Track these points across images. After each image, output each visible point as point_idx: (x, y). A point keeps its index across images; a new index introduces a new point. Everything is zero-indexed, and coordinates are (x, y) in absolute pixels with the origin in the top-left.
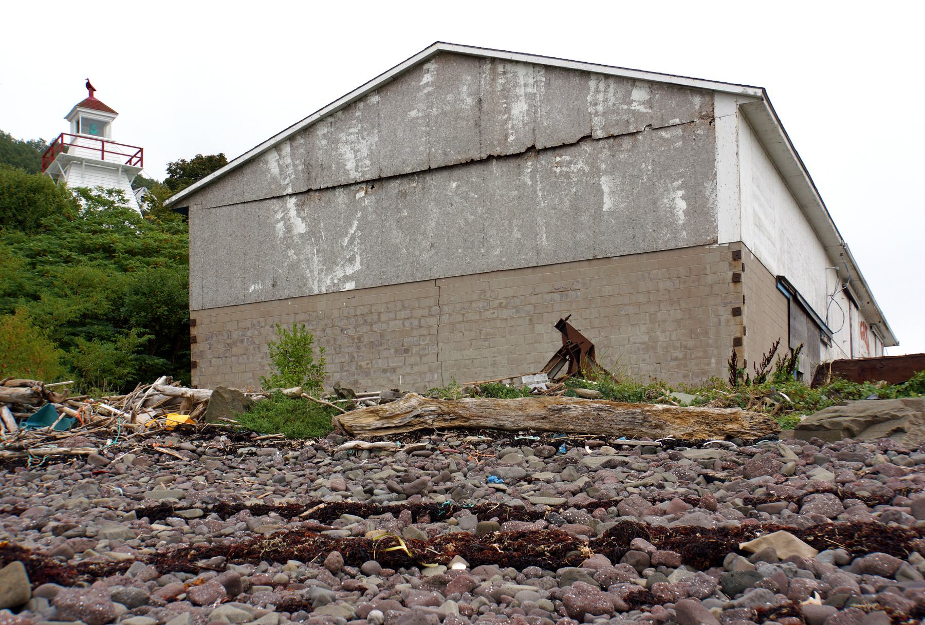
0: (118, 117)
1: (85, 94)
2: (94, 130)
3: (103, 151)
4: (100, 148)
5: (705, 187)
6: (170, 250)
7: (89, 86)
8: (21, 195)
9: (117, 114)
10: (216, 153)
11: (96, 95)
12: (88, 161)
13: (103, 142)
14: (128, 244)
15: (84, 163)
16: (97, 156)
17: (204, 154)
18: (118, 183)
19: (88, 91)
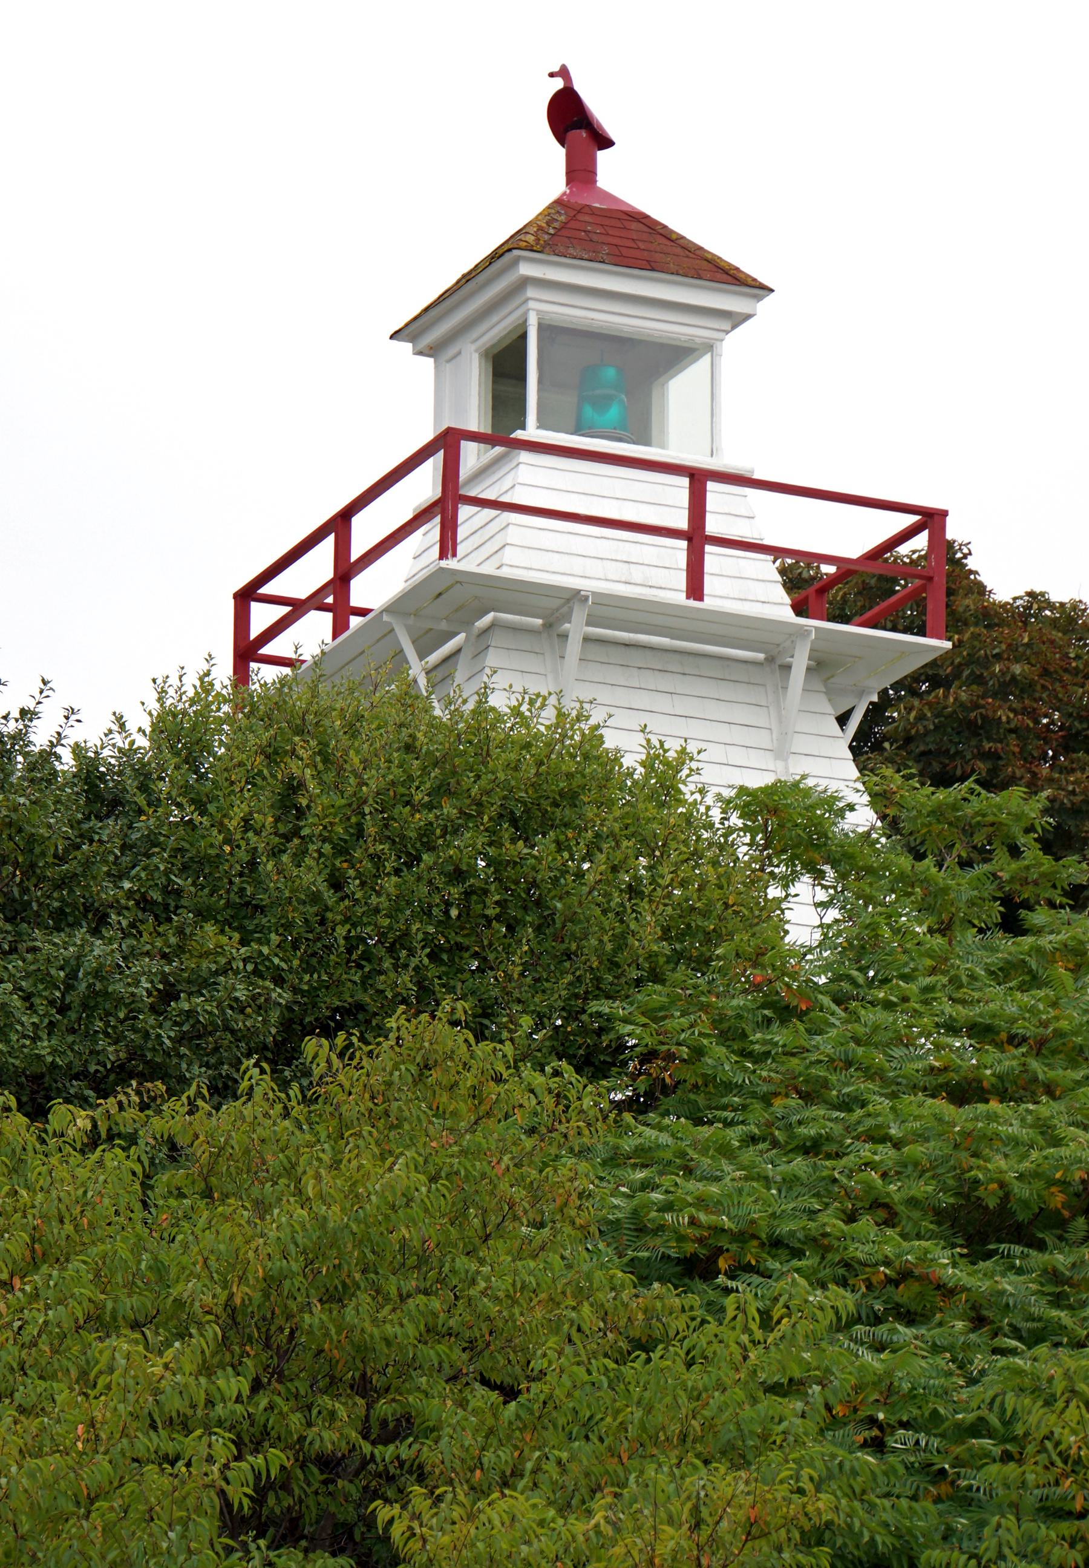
0: (764, 306)
1: (541, 174)
2: (602, 403)
3: (696, 537)
7: (569, 116)
9: (759, 289)
11: (612, 173)
12: (610, 610)
13: (698, 480)
15: (577, 627)
16: (655, 571)
17: (1057, 596)
18: (781, 752)
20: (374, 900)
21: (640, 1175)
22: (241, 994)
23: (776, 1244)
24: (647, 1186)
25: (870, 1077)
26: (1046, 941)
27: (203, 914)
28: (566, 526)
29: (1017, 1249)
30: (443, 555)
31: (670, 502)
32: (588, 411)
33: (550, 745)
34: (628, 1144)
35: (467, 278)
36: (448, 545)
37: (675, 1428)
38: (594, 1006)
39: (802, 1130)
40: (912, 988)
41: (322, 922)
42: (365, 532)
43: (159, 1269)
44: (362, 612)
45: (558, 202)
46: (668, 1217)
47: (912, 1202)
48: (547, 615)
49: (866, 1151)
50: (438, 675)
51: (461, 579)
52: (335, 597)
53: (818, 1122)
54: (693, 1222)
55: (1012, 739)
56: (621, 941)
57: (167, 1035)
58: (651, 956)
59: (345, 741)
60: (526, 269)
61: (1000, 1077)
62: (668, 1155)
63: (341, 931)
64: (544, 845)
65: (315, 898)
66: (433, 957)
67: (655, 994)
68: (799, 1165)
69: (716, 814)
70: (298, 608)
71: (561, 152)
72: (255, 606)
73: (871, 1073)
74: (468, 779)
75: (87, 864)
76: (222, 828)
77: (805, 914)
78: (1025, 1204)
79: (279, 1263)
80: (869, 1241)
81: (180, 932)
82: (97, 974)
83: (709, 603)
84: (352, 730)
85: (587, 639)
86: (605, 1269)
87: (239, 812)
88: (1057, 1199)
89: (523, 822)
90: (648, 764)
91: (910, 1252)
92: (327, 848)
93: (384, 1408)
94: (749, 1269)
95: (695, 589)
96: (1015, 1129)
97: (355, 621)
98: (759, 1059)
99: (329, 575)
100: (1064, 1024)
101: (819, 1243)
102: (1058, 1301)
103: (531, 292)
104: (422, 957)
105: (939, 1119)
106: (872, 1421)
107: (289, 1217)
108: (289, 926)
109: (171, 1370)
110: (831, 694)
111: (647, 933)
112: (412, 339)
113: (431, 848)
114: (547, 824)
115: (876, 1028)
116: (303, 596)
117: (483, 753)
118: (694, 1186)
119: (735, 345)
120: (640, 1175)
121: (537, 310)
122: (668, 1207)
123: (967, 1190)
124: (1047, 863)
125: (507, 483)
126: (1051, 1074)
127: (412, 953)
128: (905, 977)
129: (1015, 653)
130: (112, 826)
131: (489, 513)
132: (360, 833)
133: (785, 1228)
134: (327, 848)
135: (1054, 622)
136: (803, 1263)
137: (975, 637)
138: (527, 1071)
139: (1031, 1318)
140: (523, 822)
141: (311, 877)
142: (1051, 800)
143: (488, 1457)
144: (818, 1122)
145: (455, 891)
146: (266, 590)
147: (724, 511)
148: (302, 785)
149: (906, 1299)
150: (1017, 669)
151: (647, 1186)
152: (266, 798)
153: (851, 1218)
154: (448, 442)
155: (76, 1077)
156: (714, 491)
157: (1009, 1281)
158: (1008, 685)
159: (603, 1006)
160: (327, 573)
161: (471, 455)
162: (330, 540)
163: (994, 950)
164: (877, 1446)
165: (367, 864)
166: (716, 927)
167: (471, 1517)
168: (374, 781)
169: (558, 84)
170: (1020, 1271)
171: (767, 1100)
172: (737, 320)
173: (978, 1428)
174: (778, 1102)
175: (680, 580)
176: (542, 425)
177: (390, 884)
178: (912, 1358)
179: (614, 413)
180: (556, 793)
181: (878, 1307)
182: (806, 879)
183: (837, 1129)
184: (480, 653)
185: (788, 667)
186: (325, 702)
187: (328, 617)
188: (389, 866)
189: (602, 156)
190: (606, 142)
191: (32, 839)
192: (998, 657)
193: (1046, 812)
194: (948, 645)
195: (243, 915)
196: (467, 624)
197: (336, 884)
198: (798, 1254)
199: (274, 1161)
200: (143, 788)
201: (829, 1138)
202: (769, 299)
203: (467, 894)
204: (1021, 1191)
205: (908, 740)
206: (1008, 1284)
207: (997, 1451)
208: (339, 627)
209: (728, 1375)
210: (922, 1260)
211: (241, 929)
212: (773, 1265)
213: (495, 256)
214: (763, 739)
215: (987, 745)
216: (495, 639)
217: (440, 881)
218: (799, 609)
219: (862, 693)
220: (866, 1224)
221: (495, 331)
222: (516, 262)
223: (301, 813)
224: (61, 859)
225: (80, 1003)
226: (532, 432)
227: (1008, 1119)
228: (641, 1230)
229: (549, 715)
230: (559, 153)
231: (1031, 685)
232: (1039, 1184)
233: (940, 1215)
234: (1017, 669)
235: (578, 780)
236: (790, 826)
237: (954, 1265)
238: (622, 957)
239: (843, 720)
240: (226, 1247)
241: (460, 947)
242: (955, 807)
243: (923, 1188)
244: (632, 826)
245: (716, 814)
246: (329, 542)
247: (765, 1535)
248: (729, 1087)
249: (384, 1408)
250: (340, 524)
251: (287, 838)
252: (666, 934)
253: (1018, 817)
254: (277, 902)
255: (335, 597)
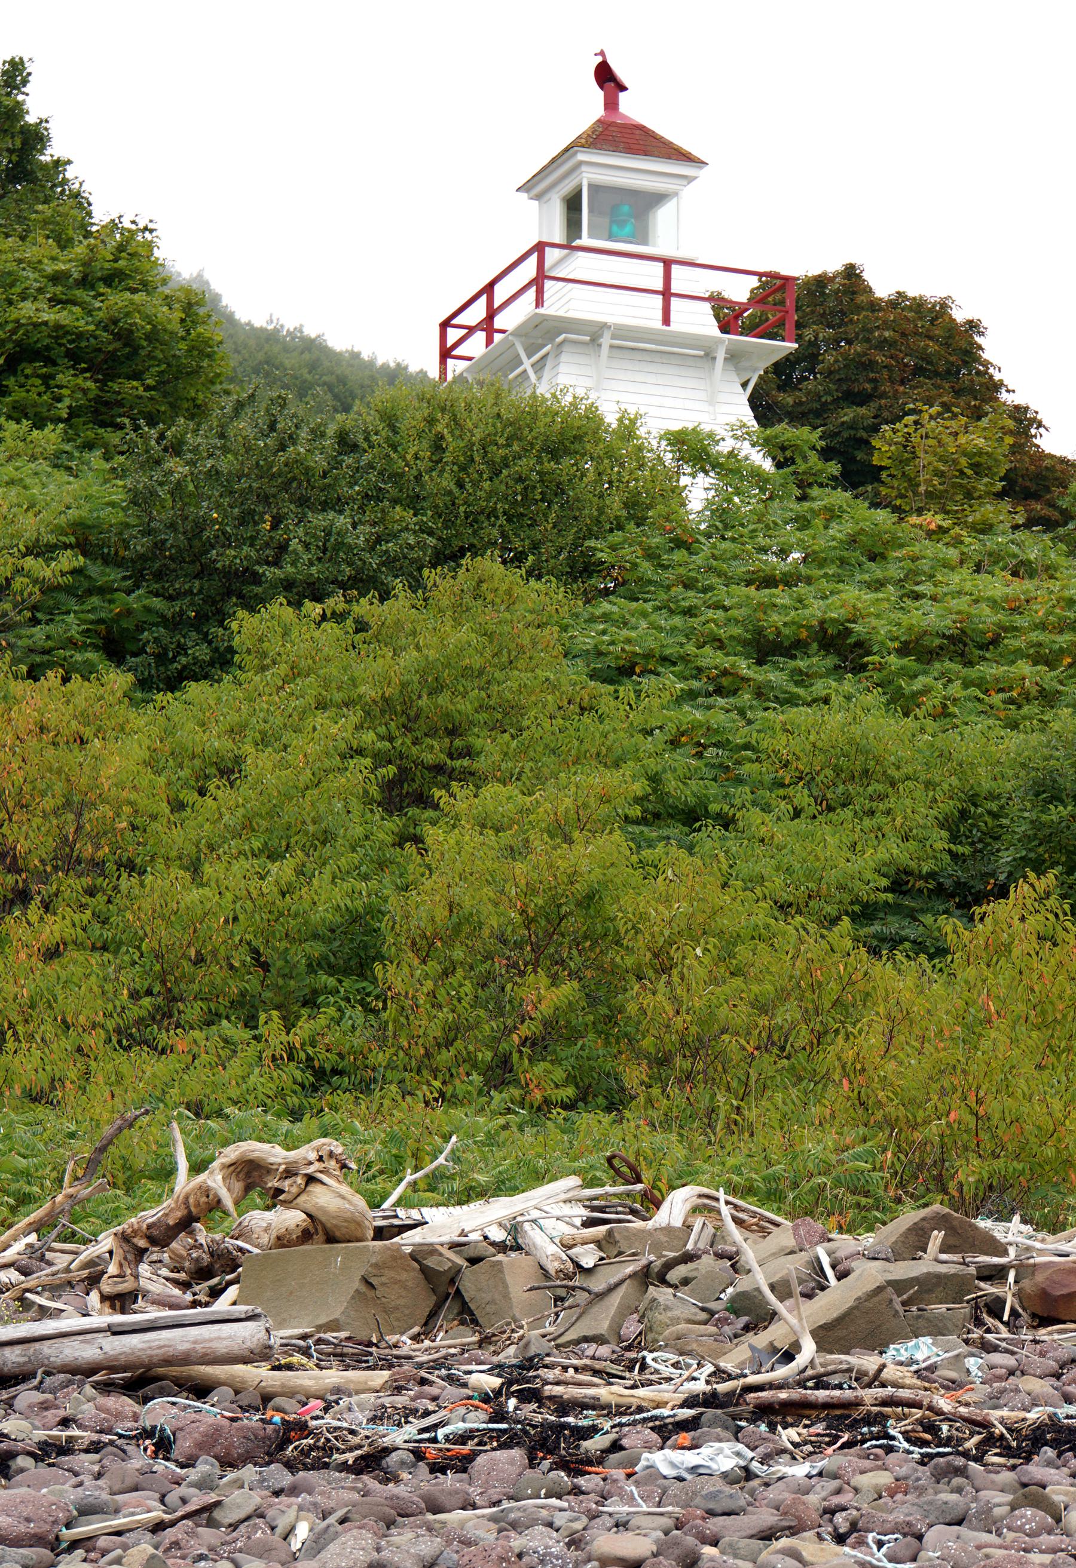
0: (703, 173)
1: (592, 104)
2: (622, 224)
3: (667, 294)
4: (659, 286)
5: (747, 458)
6: (1036, 636)
7: (605, 75)
8: (524, 464)
9: (699, 163)
10: (833, 265)
11: (630, 106)
12: (622, 332)
13: (668, 264)
14: (905, 620)
15: (606, 341)
16: (645, 312)
17: (911, 294)
18: (712, 401)
19: (599, 95)
20: (479, 493)
21: (602, 627)
22: (411, 542)
23: (665, 660)
24: (604, 632)
25: (719, 576)
26: (816, 505)
27: (395, 501)
28: (600, 289)
29: (781, 659)
30: (537, 306)
31: (652, 275)
32: (615, 228)
33: (569, 413)
34: (598, 612)
35: (553, 160)
36: (539, 301)
37: (593, 751)
38: (587, 543)
39: (683, 603)
40: (745, 531)
41: (453, 504)
42: (501, 293)
43: (353, 680)
44: (503, 332)
45: (599, 121)
46: (611, 648)
47: (732, 637)
48: (592, 336)
49: (710, 614)
50: (538, 366)
51: (546, 318)
52: (487, 325)
53: (692, 598)
54: (623, 650)
55: (885, 372)
56: (601, 511)
57: (374, 562)
58: (617, 517)
59: (465, 414)
60: (581, 157)
61: (784, 574)
62: (616, 617)
63: (462, 509)
64: (567, 461)
65: (450, 493)
66: (509, 520)
67: (617, 537)
68: (677, 621)
69: (654, 443)
70: (471, 330)
71: (601, 93)
72: (449, 330)
73: (720, 574)
74: (526, 431)
75: (336, 479)
76: (404, 458)
77: (698, 492)
78: (788, 637)
79: (407, 677)
80: (711, 658)
81: (383, 511)
82: (338, 534)
83: (675, 326)
84: (468, 408)
85: (612, 347)
86: (573, 673)
87: (412, 451)
88: (804, 634)
89: (555, 452)
90: (620, 420)
91: (727, 662)
92: (455, 468)
93: (458, 743)
94: (651, 672)
95: (666, 321)
96: (787, 601)
97: (497, 337)
98: (665, 567)
99: (484, 315)
100: (816, 548)
101: (685, 659)
102: (798, 683)
103: (584, 168)
104: (502, 521)
105: (748, 597)
106: (699, 744)
107: (410, 657)
108: (436, 507)
109: (339, 728)
110: (738, 370)
111: (615, 505)
112: (528, 191)
113: (507, 466)
114: (567, 452)
115: (725, 551)
116: (473, 324)
117: (535, 417)
118: (625, 633)
119: (688, 193)
120: (602, 627)
121: (587, 177)
122: (612, 643)
123: (759, 632)
124: (820, 465)
125: (571, 268)
126: (809, 572)
127: (497, 518)
128: (742, 525)
129: (886, 325)
130: (348, 460)
131: (561, 284)
132: (472, 460)
133: (668, 652)
134: (455, 468)
135: (910, 309)
136: (676, 668)
137: (866, 317)
138: (532, 582)
139: (786, 692)
140: (555, 452)
141: (447, 482)
142: (824, 432)
143: (504, 766)
144: (692, 598)
145: (519, 488)
146: (454, 322)
147: (682, 279)
148: (443, 437)
149: (724, 685)
150: (887, 334)
151: (604, 632)
152: (425, 444)
153: (700, 647)
154: (540, 248)
155: (333, 583)
156: (675, 268)
157: (774, 676)
158: (882, 343)
159: (592, 543)
160: (483, 314)
161: (552, 255)
162: (484, 297)
163: (387, 638)
164: (699, 755)
165: (476, 475)
166: (647, 505)
167: (476, 796)
168: (478, 434)
169: (600, 59)
170: (782, 670)
171: (668, 588)
172: (690, 179)
173: (747, 746)
174: (674, 589)
175: (659, 314)
176: (590, 236)
177: (486, 485)
178: (718, 715)
179: (628, 229)
180: (573, 436)
181: (711, 689)
182: (702, 475)
183: (700, 602)
184: (558, 355)
185: (714, 358)
186: (455, 396)
187: (484, 334)
188: (485, 476)
189: (622, 96)
190: (623, 88)
191: (308, 469)
192: (878, 327)
193: (821, 438)
194: (796, 346)
195: (414, 502)
196: (552, 340)
197: (461, 485)
198: (674, 664)
199: (408, 627)
200: (367, 439)
201: (696, 607)
202: (707, 168)
203: (526, 488)
204: (786, 631)
205: (831, 373)
206: (771, 677)
207: (754, 757)
208: (489, 341)
209: (619, 726)
210: (733, 665)
211: (414, 508)
212: (661, 669)
213: (567, 150)
214: (702, 395)
215: (872, 375)
216: (566, 348)
217: (511, 483)
218: (724, 328)
219: (755, 370)
220: (707, 649)
221: (567, 188)
222: (576, 152)
223: (444, 450)
224: (324, 476)
225: (330, 547)
226: (585, 240)
227: (781, 596)
228: (600, 654)
229: (569, 398)
230: (600, 94)
231: (896, 342)
232: (794, 627)
233: (745, 643)
234: (887, 334)
235: (584, 429)
236: (693, 449)
237: (749, 668)
238: (603, 518)
239: (744, 385)
240: (378, 672)
241: (522, 515)
242: (776, 437)
243: (737, 631)
244: (610, 453)
245: (654, 443)
246: (484, 298)
247: (609, 801)
248: (650, 582)
249: (458, 743)
250: (489, 289)
251: (437, 462)
252: (626, 505)
253: (806, 441)
254: (430, 495)
255: (487, 325)
